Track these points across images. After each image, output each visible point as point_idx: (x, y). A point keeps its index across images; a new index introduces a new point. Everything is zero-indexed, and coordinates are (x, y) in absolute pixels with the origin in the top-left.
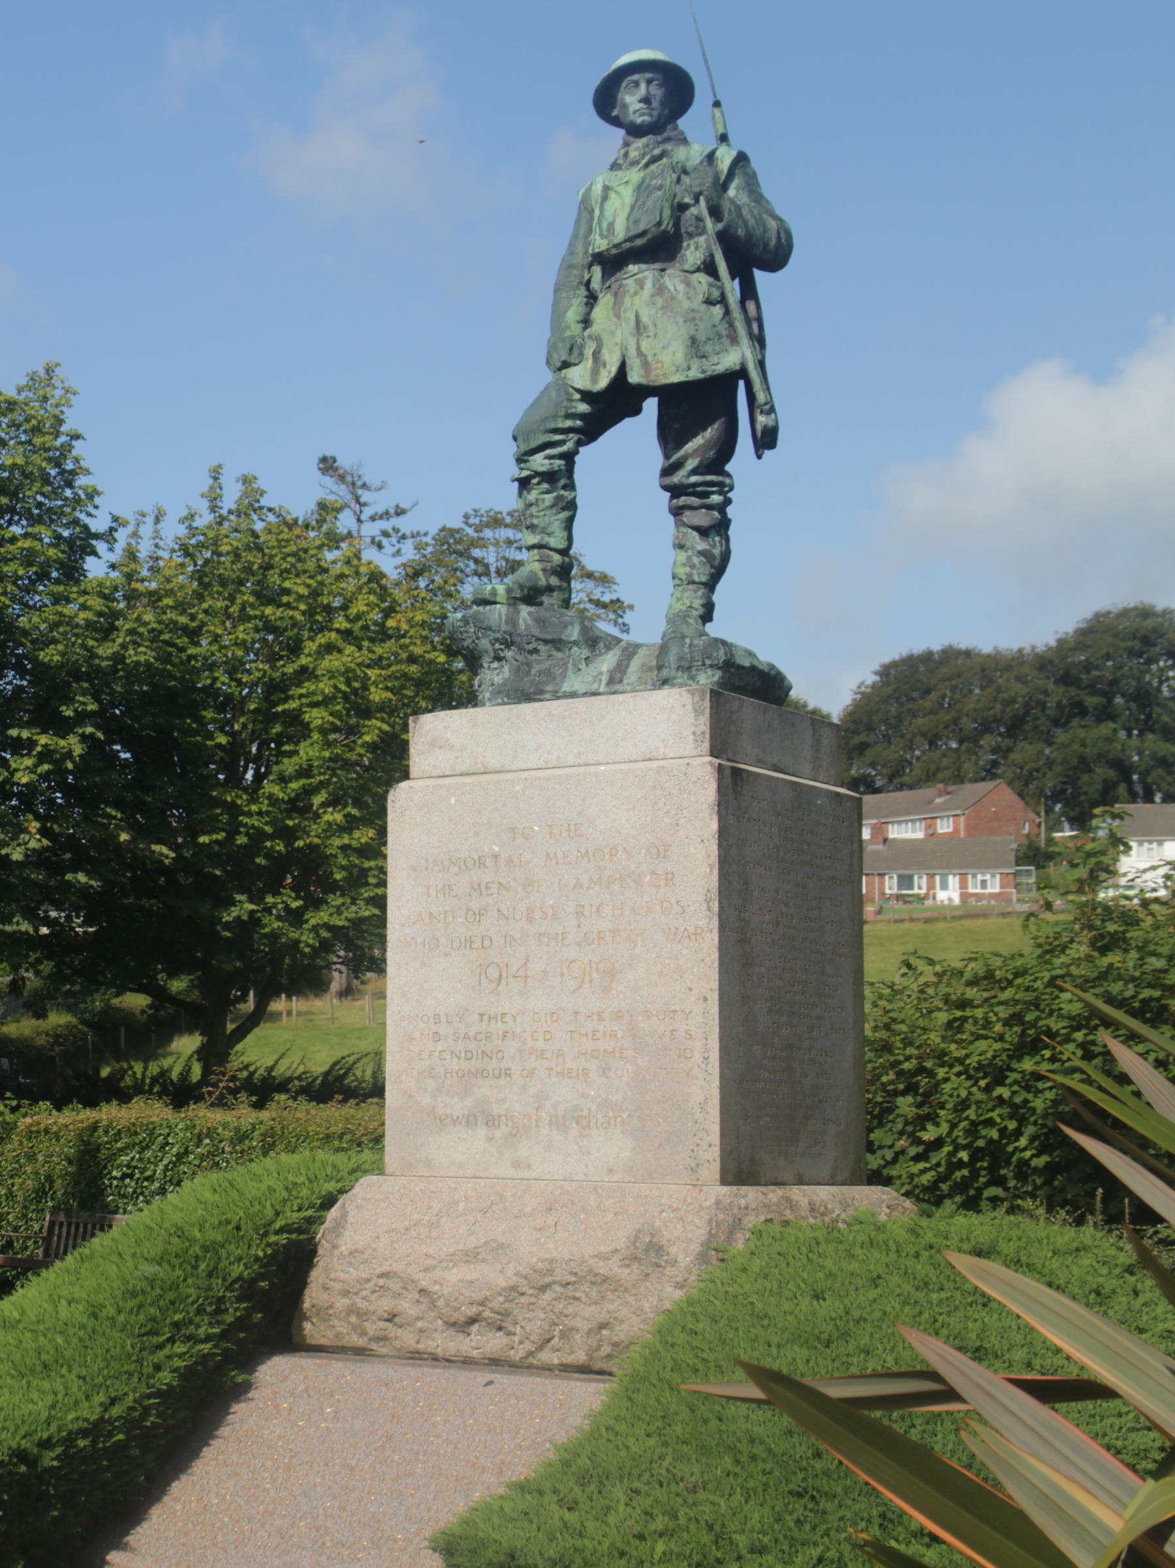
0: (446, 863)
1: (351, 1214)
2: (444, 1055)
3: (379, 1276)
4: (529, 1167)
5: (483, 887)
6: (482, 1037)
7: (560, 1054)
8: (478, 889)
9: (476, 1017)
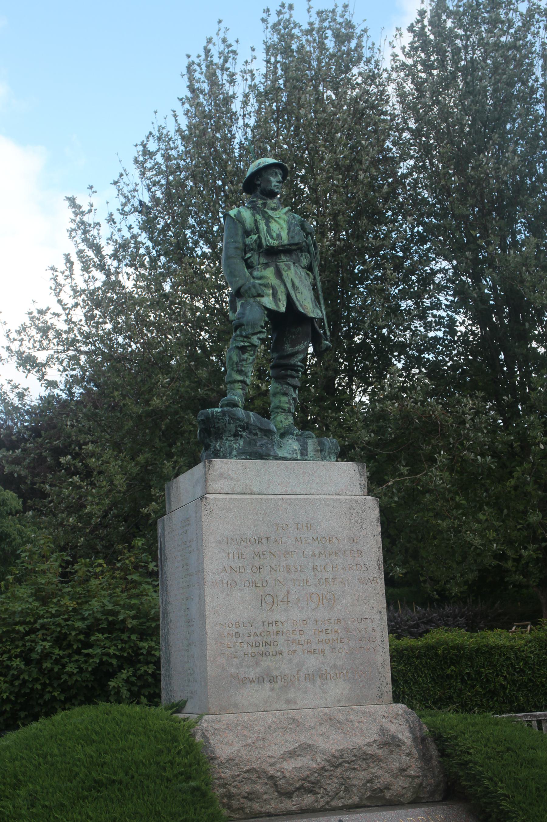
0: (239, 540)
1: (211, 738)
2: (243, 645)
3: (245, 772)
4: (295, 703)
5: (261, 554)
6: (265, 634)
7: (309, 642)
8: (257, 554)
9: (261, 624)
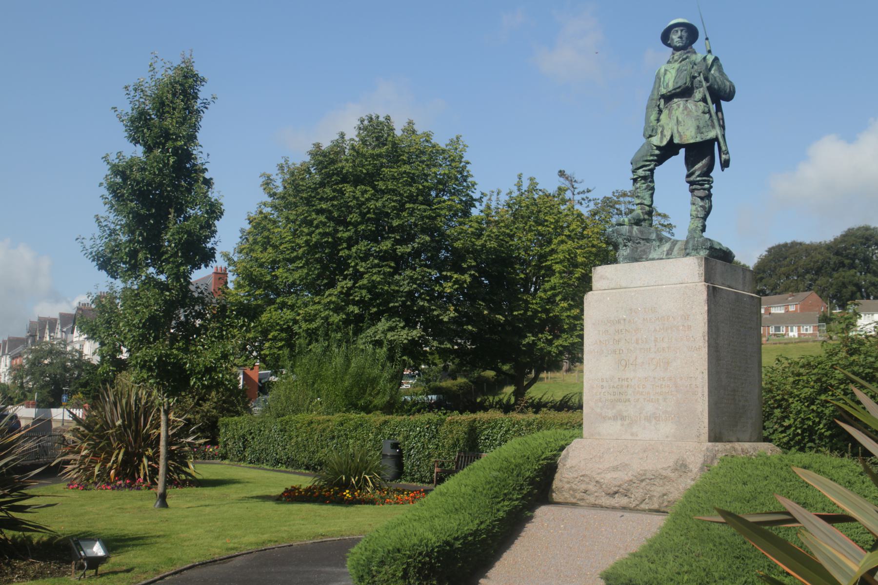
8: (618, 331)
